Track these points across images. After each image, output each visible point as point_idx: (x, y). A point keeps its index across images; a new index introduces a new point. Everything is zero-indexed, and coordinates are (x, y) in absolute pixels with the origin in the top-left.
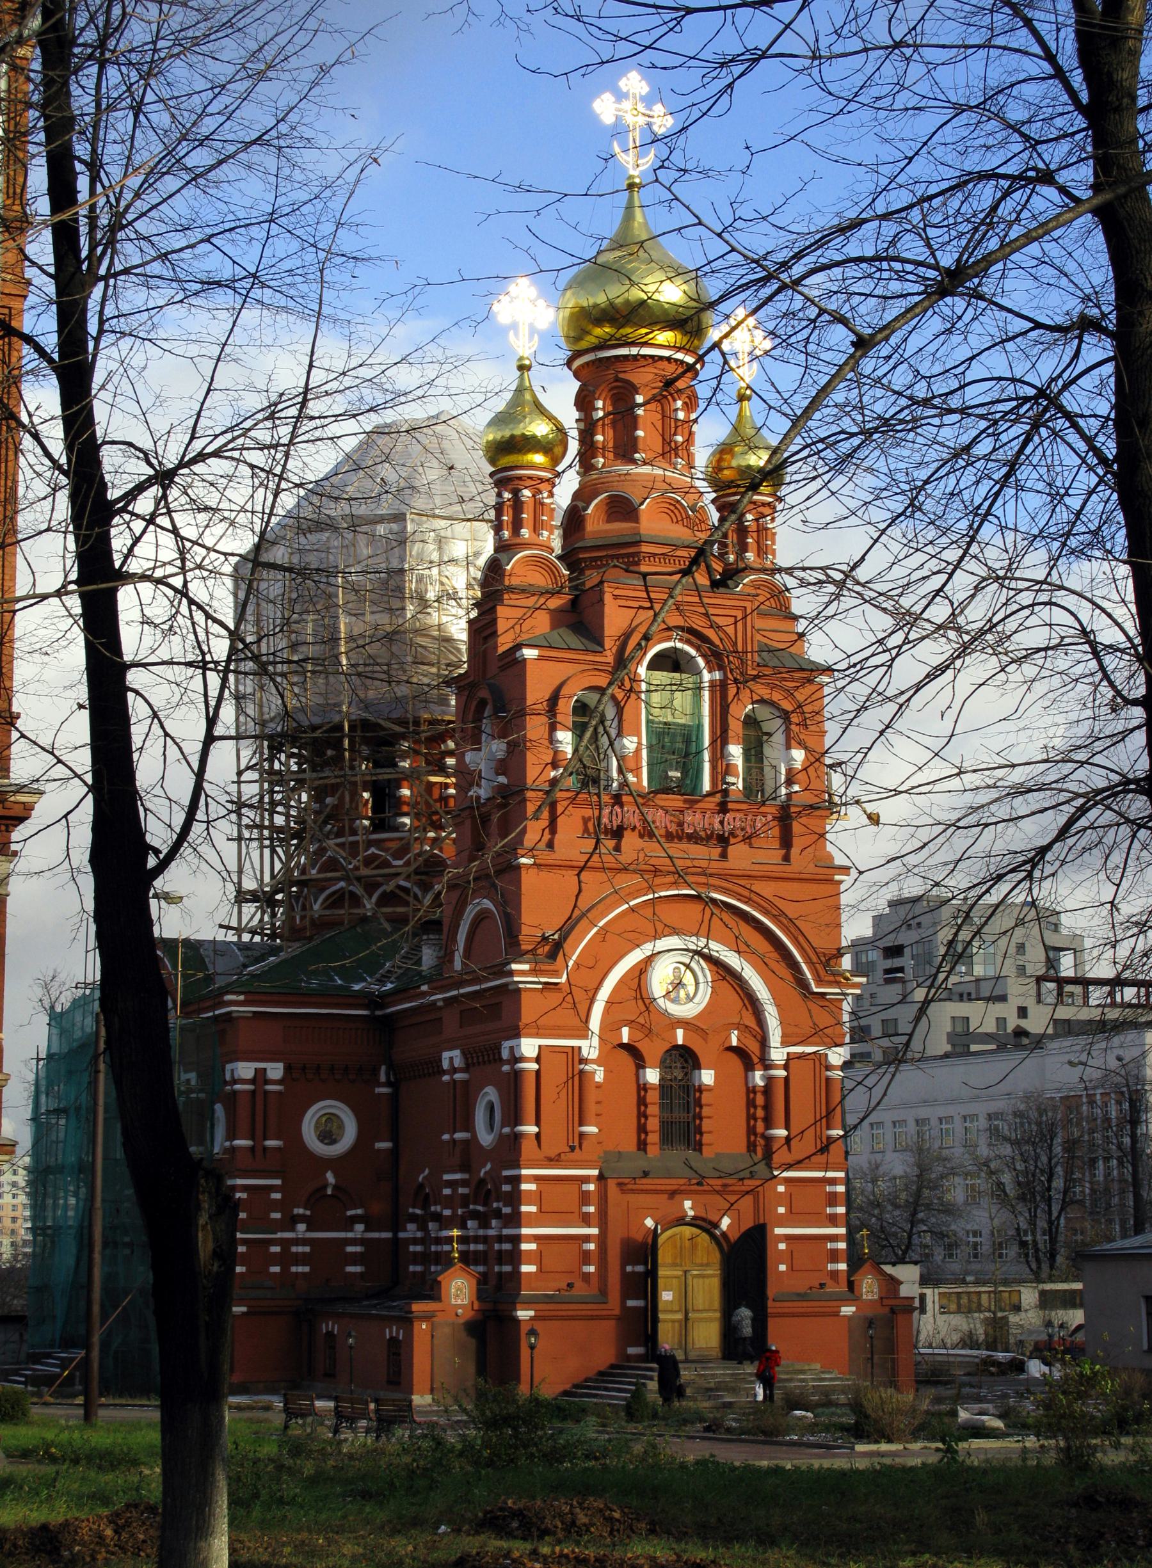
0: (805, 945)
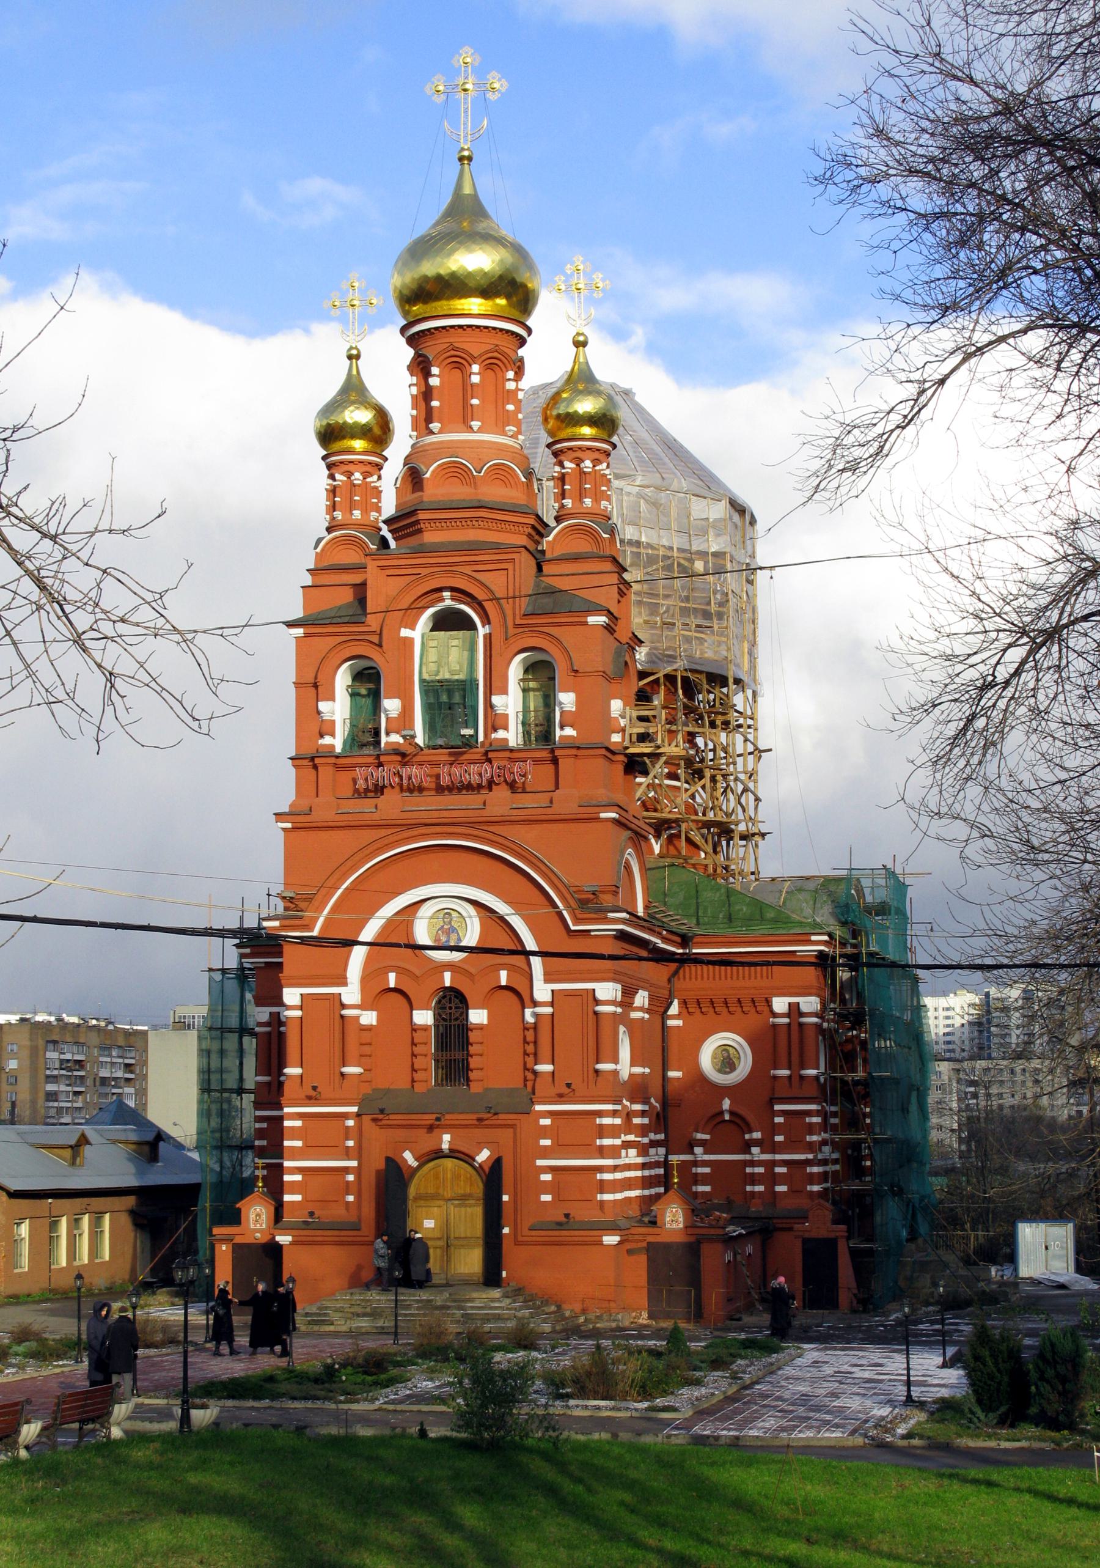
0: (559, 885)
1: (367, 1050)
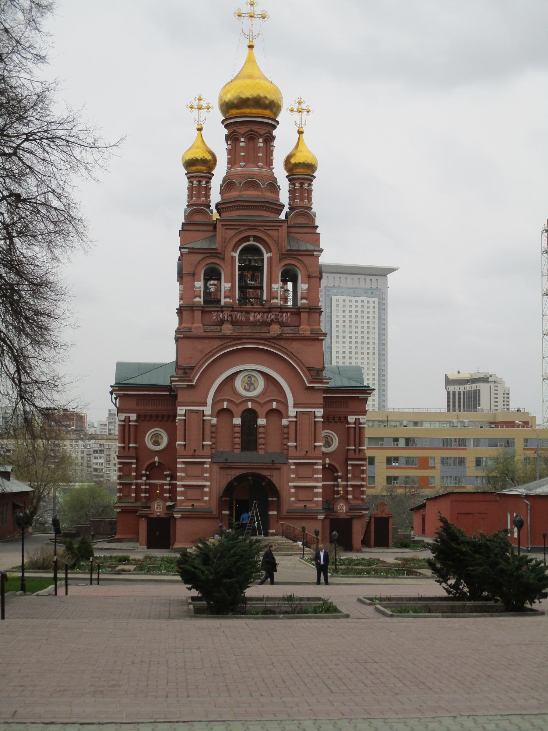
1: (214, 435)
